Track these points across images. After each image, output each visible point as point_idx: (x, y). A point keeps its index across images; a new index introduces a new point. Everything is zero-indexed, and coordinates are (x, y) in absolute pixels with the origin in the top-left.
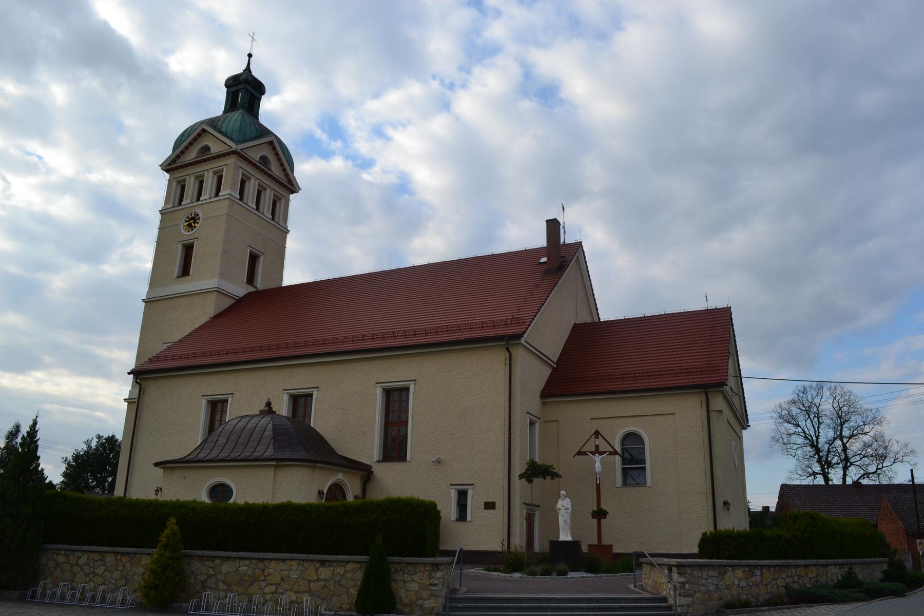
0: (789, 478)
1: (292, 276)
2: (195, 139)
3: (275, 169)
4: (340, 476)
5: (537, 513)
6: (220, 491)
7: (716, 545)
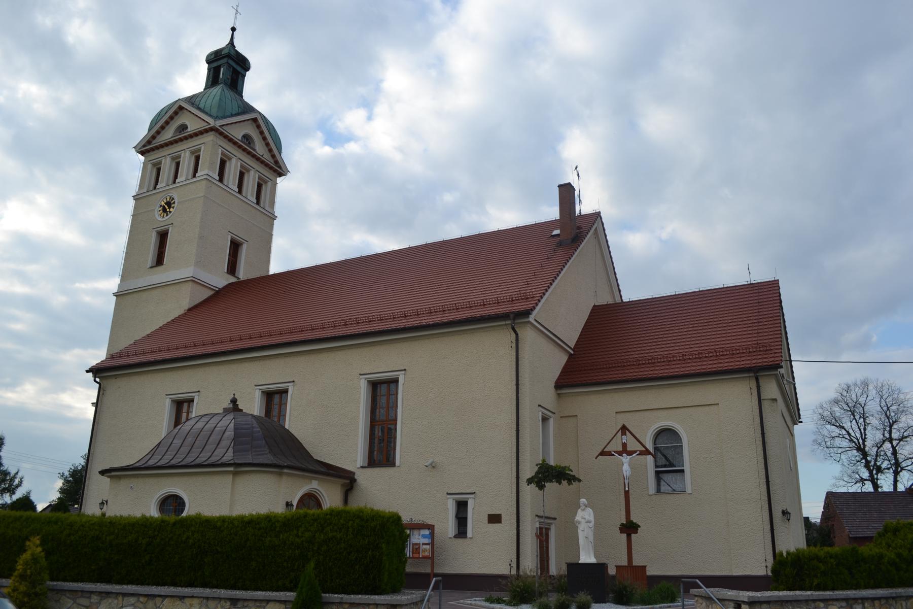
0: (835, 485)
1: (275, 268)
2: (171, 118)
3: (260, 148)
4: (314, 485)
5: (553, 528)
6: (172, 503)
7: (789, 571)
